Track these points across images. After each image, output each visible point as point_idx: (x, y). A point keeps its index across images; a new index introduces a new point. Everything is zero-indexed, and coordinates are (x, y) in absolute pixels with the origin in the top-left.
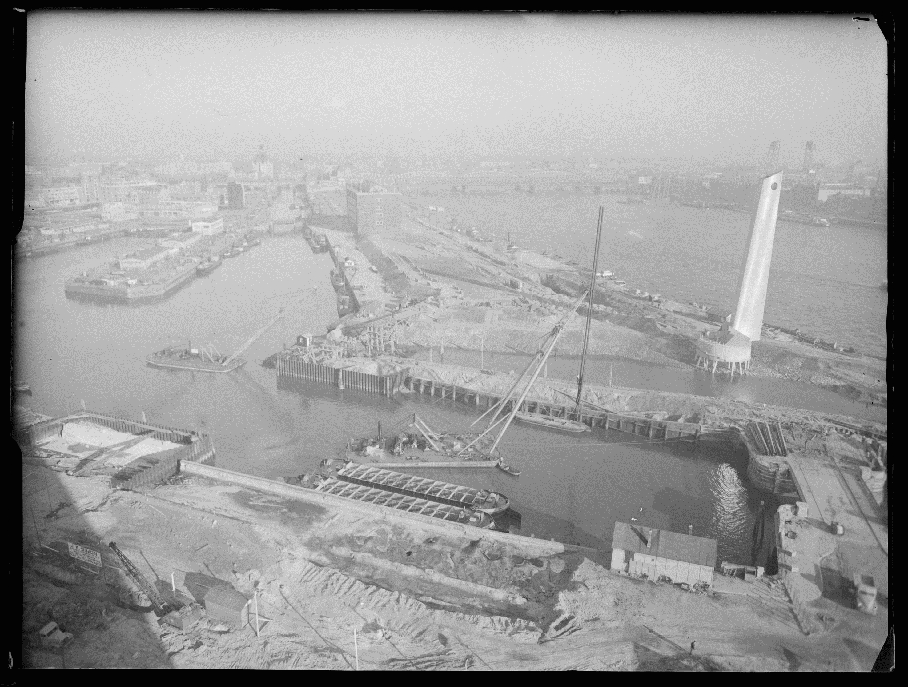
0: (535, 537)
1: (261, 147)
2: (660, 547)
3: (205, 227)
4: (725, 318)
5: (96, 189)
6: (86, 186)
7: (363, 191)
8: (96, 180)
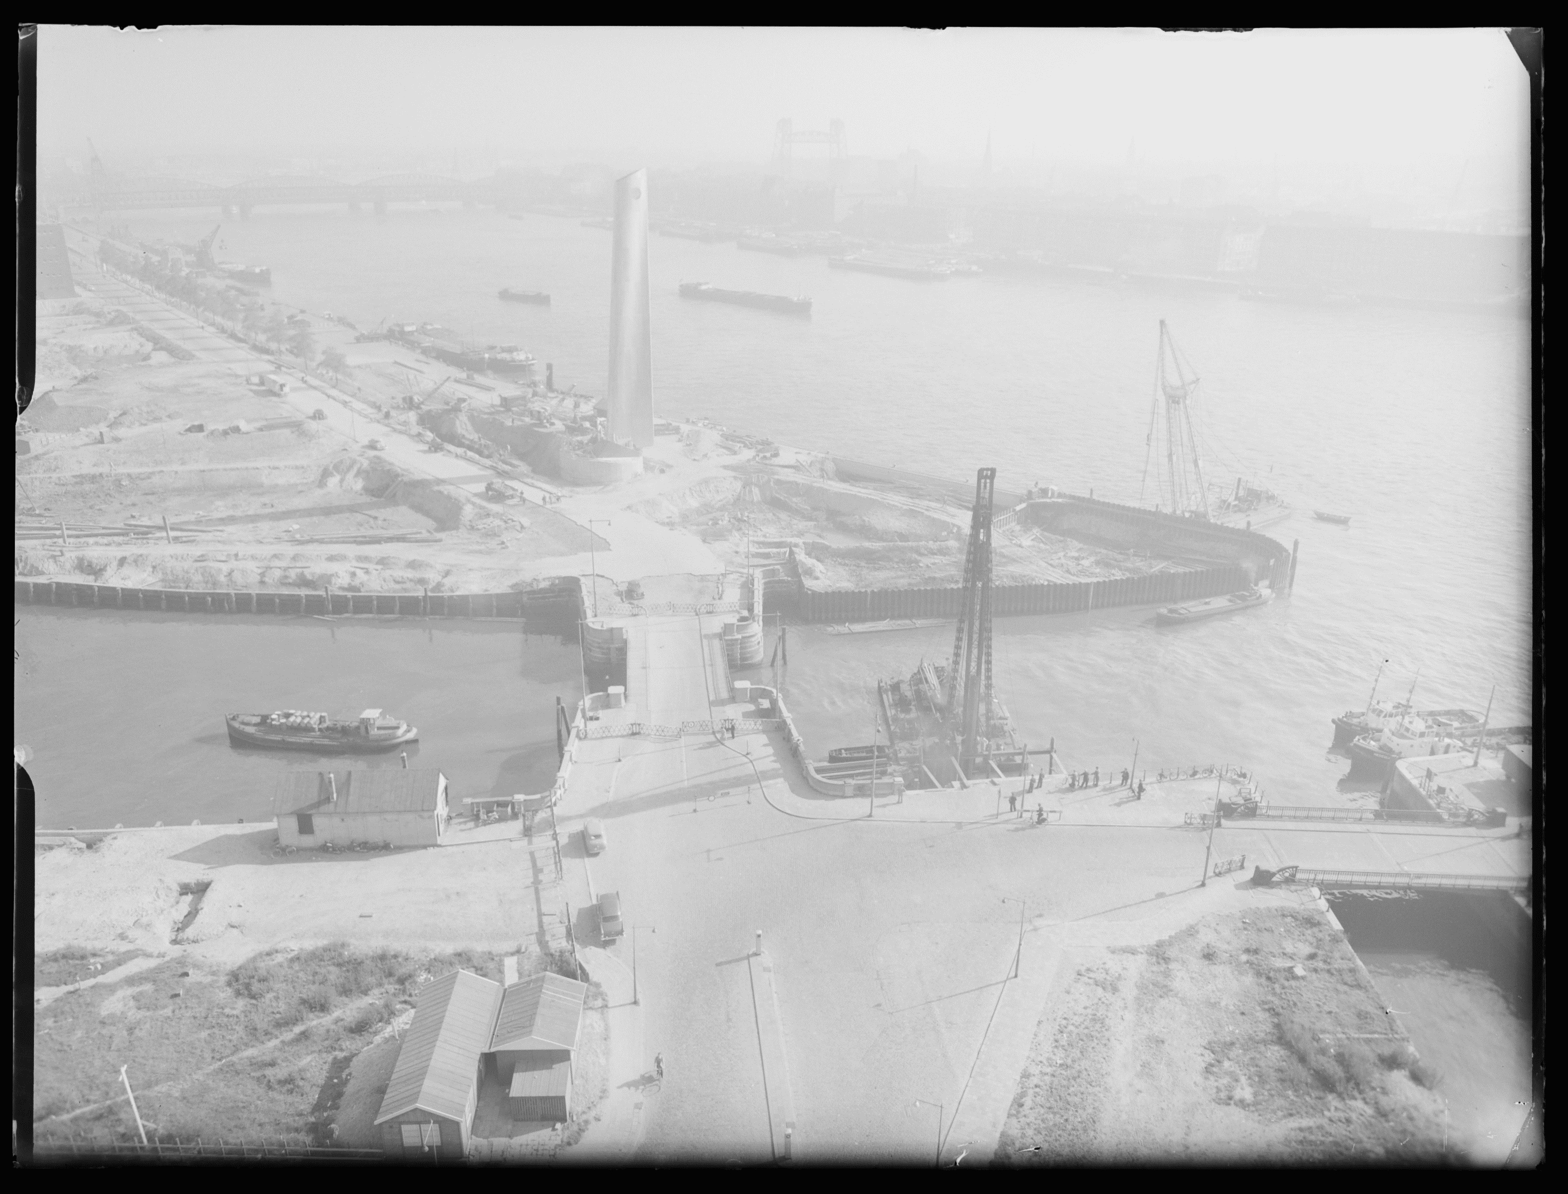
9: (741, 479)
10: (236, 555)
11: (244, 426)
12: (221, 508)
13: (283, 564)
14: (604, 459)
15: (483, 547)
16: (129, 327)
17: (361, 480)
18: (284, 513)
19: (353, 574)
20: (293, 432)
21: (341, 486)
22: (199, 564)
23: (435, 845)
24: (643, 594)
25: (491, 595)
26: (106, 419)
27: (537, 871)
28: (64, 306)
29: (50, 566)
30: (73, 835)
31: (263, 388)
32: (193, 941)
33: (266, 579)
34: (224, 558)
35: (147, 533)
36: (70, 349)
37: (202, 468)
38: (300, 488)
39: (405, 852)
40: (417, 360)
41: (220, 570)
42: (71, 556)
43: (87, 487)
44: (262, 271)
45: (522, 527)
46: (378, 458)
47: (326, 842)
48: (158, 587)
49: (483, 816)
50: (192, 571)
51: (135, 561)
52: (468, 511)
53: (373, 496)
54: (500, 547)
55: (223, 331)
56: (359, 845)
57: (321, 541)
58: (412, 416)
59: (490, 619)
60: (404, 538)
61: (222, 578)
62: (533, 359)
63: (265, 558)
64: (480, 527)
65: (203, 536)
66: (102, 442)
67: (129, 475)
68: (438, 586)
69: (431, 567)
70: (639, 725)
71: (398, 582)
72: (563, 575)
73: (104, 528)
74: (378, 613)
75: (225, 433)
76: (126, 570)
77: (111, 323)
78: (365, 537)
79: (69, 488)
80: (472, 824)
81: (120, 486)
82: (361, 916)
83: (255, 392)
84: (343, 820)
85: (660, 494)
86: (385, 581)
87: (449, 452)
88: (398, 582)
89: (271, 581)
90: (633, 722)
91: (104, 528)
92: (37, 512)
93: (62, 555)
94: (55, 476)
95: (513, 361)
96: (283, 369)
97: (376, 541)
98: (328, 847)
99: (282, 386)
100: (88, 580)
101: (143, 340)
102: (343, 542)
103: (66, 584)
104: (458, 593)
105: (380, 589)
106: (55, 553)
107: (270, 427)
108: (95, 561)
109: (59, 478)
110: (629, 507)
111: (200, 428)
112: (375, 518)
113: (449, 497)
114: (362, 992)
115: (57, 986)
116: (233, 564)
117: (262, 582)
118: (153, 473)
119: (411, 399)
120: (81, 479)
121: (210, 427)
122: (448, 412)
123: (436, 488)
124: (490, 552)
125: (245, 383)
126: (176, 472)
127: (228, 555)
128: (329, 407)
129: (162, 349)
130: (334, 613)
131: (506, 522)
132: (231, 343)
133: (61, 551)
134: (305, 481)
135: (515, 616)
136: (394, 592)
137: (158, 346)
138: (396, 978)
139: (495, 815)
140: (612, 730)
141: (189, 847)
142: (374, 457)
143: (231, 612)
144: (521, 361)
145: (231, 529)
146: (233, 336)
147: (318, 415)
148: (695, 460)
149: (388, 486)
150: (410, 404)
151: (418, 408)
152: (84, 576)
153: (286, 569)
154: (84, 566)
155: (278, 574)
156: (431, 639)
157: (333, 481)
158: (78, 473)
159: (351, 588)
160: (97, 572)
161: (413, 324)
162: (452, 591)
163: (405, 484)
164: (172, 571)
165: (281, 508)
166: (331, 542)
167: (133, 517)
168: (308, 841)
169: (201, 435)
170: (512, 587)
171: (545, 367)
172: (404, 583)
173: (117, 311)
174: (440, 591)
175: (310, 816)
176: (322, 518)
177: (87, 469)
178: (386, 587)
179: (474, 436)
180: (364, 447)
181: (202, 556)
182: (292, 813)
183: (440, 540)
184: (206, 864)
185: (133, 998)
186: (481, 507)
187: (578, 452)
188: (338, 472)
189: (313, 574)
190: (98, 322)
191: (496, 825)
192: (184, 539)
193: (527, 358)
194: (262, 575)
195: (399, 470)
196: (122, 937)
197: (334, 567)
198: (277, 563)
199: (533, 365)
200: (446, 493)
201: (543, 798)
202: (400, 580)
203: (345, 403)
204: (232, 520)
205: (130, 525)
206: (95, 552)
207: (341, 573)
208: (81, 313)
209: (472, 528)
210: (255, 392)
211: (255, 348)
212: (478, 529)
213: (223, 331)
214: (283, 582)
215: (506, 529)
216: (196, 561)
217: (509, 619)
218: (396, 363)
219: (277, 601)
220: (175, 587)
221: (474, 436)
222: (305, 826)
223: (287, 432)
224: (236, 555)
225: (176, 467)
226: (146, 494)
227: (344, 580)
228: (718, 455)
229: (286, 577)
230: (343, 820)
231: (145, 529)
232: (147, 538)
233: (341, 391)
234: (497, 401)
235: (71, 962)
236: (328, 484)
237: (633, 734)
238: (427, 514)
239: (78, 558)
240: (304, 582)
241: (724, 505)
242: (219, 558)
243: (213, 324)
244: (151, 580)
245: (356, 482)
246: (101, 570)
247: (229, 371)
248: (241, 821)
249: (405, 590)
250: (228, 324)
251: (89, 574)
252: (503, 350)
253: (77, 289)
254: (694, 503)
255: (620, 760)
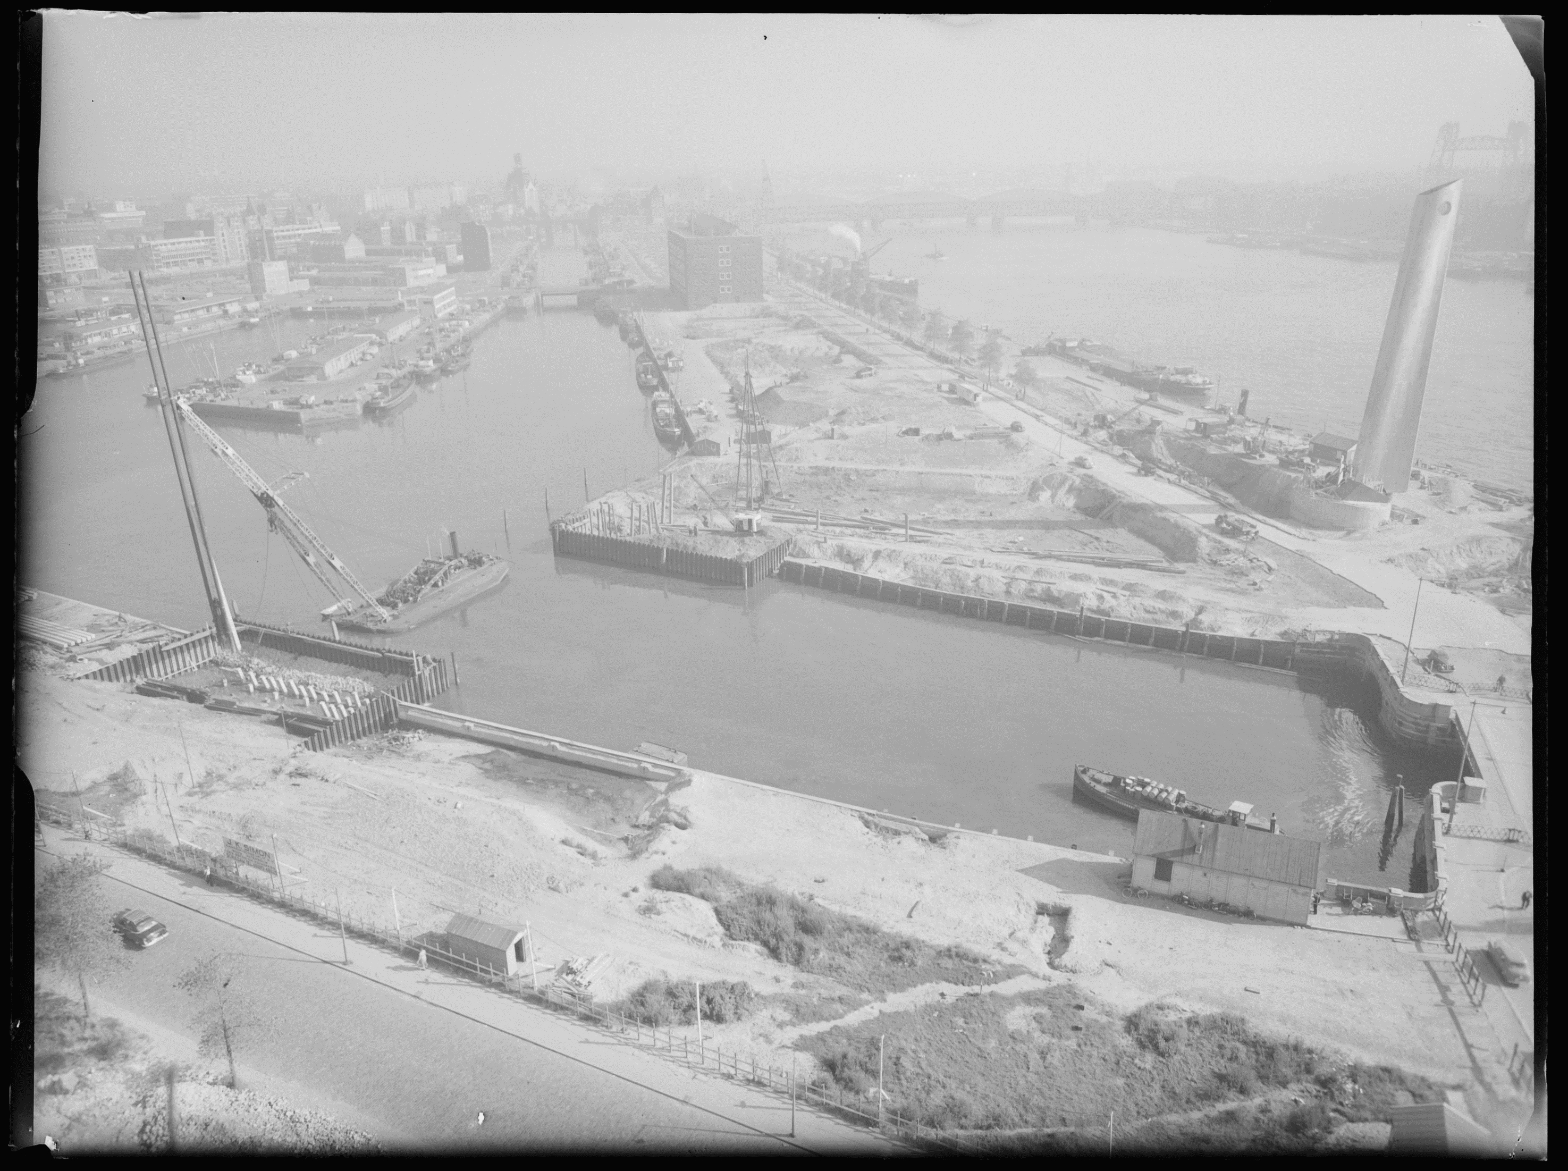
0: (1000, 834)
1: (518, 158)
2: (1217, 854)
3: (425, 303)
4: (1345, 453)
5: (240, 239)
6: (223, 234)
7: (407, 255)
8: (221, 225)
9: (1520, 541)
10: (982, 562)
11: (957, 435)
12: (942, 512)
13: (1028, 577)
14: (1350, 502)
15: (1233, 586)
16: (816, 330)
17: (1072, 497)
18: (1003, 522)
19: (1101, 598)
20: (1001, 443)
21: (1053, 502)
22: (947, 566)
23: (1304, 926)
24: (1452, 668)
25: (1259, 641)
26: (827, 415)
27: (1444, 989)
28: (754, 310)
29: (815, 551)
30: (918, 826)
31: (955, 396)
32: (1071, 971)
33: (1012, 590)
34: (969, 564)
35: (885, 529)
36: (771, 349)
37: (920, 470)
38: (1012, 499)
39: (1269, 925)
40: (1088, 377)
41: (967, 575)
42: (832, 543)
43: (822, 478)
44: (911, 282)
45: (1270, 569)
46: (1091, 477)
47: (1182, 894)
48: (910, 583)
49: (1356, 904)
50: (941, 573)
51: (889, 556)
52: (1204, 546)
53: (1089, 515)
54: (1252, 587)
55: (898, 338)
56: (1219, 905)
57: (1059, 558)
58: (1102, 434)
59: (1254, 666)
60: (1145, 565)
61: (969, 583)
62: (1210, 383)
63: (1009, 569)
64: (1224, 563)
65: (935, 538)
66: (832, 438)
67: (857, 471)
68: (1195, 622)
69: (1184, 600)
70: (1520, 832)
71: (1148, 612)
72: (1348, 631)
73: (845, 519)
74: (1130, 641)
75: (939, 438)
76: (881, 563)
77: (797, 327)
78: (1103, 559)
79: (807, 478)
80: (1338, 910)
81: (849, 480)
82: (1246, 990)
83: (947, 399)
84: (1205, 875)
85: (1423, 549)
86: (1135, 608)
87: (1160, 477)
88: (1148, 612)
89: (1017, 592)
90: (1512, 827)
91: (845, 519)
92: (784, 497)
93: (825, 541)
94: (795, 465)
95: (1189, 383)
96: (966, 379)
97: (1117, 565)
98: (1183, 900)
99: (976, 396)
100: (849, 568)
101: (829, 343)
102: (1082, 562)
103: (833, 570)
104: (1220, 633)
105: (1129, 616)
106: (819, 540)
107: (982, 436)
108: (853, 551)
109: (799, 468)
110: (1390, 560)
111: (916, 432)
112: (1097, 539)
113: (1177, 526)
114: (1280, 1083)
115: (956, 984)
116: (979, 570)
117: (1008, 593)
118: (877, 471)
119: (1104, 418)
120: (816, 471)
121: (924, 432)
122: (1141, 433)
123: (1159, 514)
124: (1243, 593)
125: (936, 390)
126: (897, 472)
127: (974, 561)
128: (1027, 422)
129: (848, 352)
130: (1084, 634)
131: (1251, 561)
132: (908, 350)
133: (825, 538)
134: (1015, 492)
135: (1284, 668)
136: (1144, 621)
137: (844, 350)
138: (1313, 1077)
139: (1370, 906)
140: (1483, 831)
141: (1032, 865)
142: (1084, 475)
143: (982, 618)
144: (1198, 384)
145: (958, 533)
146: (909, 343)
147: (1016, 428)
148: (1451, 512)
149: (1103, 507)
150: (1102, 422)
151: (1110, 427)
152: (843, 564)
153: (1030, 582)
154: (843, 554)
155: (1023, 586)
156: (1182, 679)
157: (1045, 496)
158: (814, 465)
159: (1100, 611)
160: (856, 562)
161: (1075, 340)
162: (1213, 630)
163: (1123, 506)
164: (922, 570)
165: (1000, 518)
166: (1069, 560)
167: (866, 511)
168: (1161, 887)
169: (917, 438)
170: (1284, 634)
171: (1240, 393)
172: (1156, 613)
173: (802, 315)
174: (1197, 628)
175: (1171, 863)
176: (1043, 531)
177: (821, 462)
178: (1135, 615)
179: (1170, 461)
180: (1070, 463)
181: (950, 558)
182: (1153, 856)
183: (1183, 572)
184: (1058, 886)
185: (1034, 1018)
186: (1216, 541)
187: (1319, 491)
188: (1049, 487)
189: (1059, 592)
190: (786, 325)
191: (1369, 917)
192: (918, 539)
193: (1204, 382)
194: (1008, 585)
195: (1115, 492)
196: (1001, 946)
197: (1079, 587)
198: (1020, 575)
199: (1209, 389)
200: (1172, 520)
201: (1426, 898)
202: (1151, 609)
203: (1037, 417)
204: (955, 524)
205: (867, 519)
206: (855, 543)
207: (1089, 595)
208: (770, 316)
209: (1215, 563)
210: (947, 399)
211: (933, 355)
212: (1221, 565)
213: (898, 338)
214: (1029, 595)
215: (1253, 568)
216: (944, 563)
217: (1278, 670)
218: (1068, 378)
219: (1029, 614)
220: (924, 586)
221: (1170, 461)
222: (1163, 870)
223: (995, 442)
224: (982, 562)
225: (896, 467)
226: (871, 490)
227: (1092, 603)
228: (1480, 510)
229: (1032, 591)
230: (1205, 875)
231: (881, 525)
232: (885, 534)
233: (1029, 404)
234: (1192, 426)
235: (965, 962)
236: (1040, 498)
237: (1509, 841)
238: (1151, 540)
239: (837, 546)
240: (1049, 598)
241: (1498, 571)
242: (965, 563)
243: (886, 331)
244: (904, 576)
245: (1068, 499)
246: (858, 560)
247: (916, 378)
248: (1074, 847)
249: (1156, 621)
250: (904, 333)
251: (847, 562)
252: (1178, 372)
253: (765, 296)
254: (1462, 564)
255: (1502, 871)
